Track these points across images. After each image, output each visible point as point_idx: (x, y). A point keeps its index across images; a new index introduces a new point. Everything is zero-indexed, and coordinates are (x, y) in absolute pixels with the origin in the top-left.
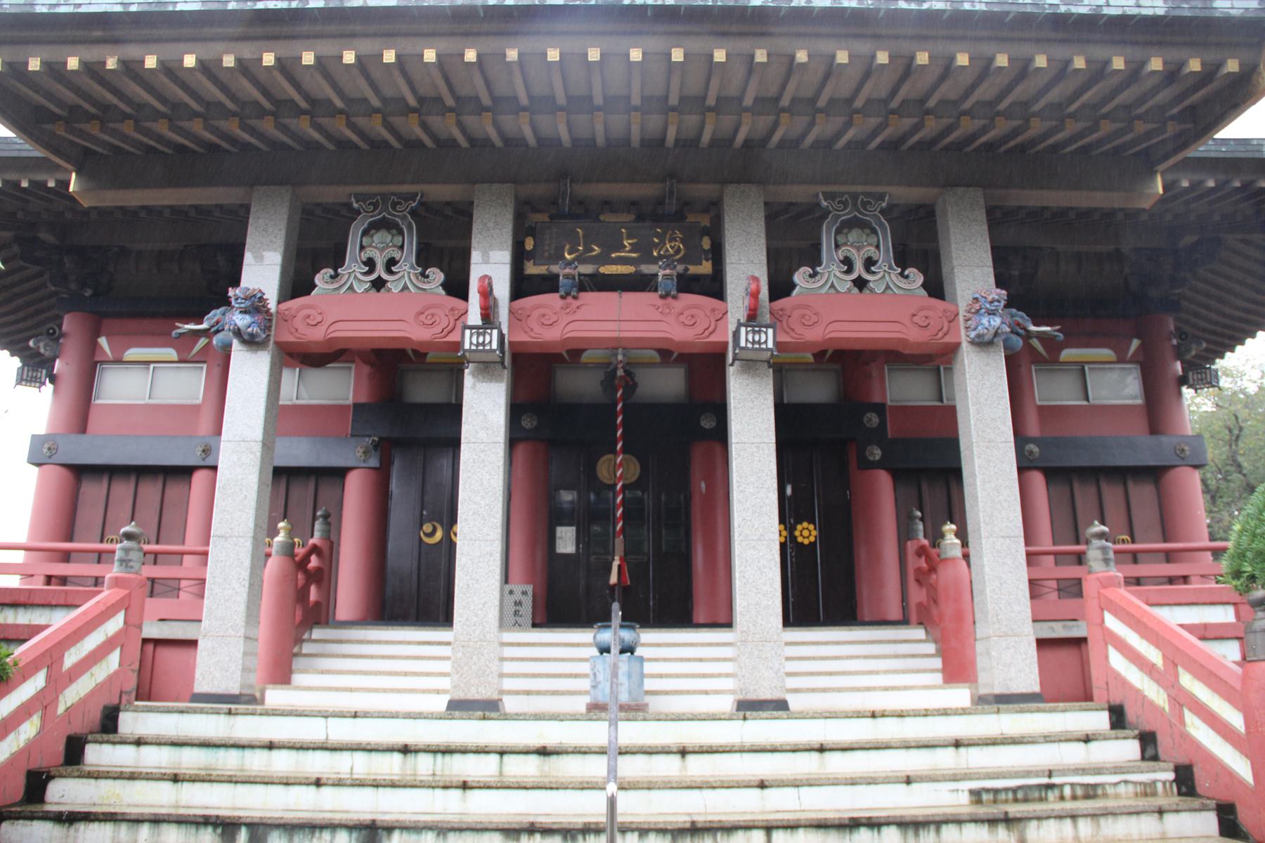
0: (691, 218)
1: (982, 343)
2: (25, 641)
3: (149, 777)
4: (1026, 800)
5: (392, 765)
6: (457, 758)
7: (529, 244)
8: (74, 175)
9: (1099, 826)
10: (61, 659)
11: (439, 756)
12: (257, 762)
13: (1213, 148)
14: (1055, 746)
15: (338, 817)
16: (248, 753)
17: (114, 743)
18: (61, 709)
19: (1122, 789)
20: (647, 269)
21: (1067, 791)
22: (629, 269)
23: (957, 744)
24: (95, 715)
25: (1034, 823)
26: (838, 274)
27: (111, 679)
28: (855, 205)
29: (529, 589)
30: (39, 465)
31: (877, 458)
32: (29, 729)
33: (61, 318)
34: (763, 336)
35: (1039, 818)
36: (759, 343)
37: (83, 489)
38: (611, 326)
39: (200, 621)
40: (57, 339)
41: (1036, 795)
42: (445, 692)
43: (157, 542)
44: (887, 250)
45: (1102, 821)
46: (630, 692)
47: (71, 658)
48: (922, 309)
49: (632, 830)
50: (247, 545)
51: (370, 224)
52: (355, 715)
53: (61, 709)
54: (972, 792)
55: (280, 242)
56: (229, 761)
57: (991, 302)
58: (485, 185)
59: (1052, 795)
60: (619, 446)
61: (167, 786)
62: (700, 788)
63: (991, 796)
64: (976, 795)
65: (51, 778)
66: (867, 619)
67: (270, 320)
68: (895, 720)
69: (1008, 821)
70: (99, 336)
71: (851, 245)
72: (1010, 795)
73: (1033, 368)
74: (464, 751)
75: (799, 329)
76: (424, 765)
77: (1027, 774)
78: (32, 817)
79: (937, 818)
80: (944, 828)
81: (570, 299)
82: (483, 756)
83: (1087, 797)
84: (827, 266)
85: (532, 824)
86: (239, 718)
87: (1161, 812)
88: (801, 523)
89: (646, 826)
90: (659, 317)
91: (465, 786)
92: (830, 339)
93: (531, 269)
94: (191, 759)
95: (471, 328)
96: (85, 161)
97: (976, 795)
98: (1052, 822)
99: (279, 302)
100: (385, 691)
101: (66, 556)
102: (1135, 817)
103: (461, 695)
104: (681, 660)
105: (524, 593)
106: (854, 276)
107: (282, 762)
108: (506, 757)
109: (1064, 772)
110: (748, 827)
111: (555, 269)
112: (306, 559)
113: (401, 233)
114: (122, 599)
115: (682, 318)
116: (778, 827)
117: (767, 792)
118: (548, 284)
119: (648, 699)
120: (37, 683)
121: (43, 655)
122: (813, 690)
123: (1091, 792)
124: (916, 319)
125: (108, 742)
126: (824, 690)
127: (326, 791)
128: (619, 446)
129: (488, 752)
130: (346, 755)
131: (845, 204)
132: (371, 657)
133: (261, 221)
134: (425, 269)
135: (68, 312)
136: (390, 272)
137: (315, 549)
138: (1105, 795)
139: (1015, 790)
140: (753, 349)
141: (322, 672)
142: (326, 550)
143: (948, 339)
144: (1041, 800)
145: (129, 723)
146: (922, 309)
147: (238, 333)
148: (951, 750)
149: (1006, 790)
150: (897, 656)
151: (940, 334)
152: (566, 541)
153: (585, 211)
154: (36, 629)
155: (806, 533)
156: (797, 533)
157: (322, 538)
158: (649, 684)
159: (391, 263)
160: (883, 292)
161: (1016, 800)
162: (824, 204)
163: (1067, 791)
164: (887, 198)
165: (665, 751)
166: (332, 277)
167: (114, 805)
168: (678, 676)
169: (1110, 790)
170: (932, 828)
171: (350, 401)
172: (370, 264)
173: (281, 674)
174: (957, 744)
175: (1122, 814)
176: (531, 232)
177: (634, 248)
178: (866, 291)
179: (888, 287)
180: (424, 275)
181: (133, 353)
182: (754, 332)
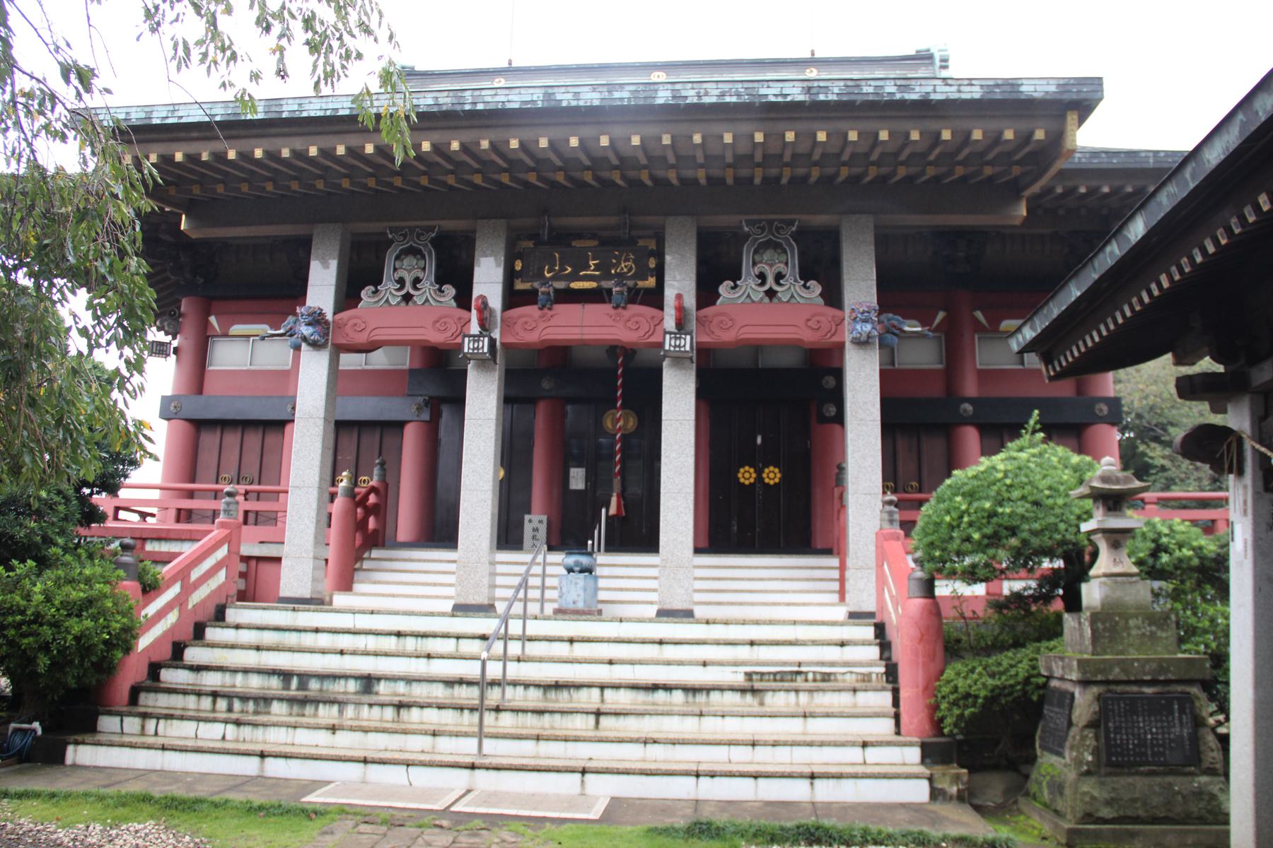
0: (641, 243)
1: (862, 343)
2: (170, 562)
3: (242, 647)
4: (782, 680)
5: (390, 643)
6: (430, 640)
7: (518, 266)
8: (184, 217)
9: (813, 697)
10: (189, 575)
11: (419, 639)
12: (308, 640)
13: (1106, 160)
14: (820, 647)
15: (348, 672)
16: (303, 634)
17: (223, 627)
18: (190, 606)
19: (848, 677)
20: (606, 284)
21: (810, 676)
22: (593, 285)
23: (752, 643)
24: (211, 610)
25: (770, 694)
26: (753, 286)
27: (220, 587)
28: (770, 229)
29: (545, 518)
30: (168, 419)
31: (833, 414)
32: (172, 617)
33: (180, 301)
34: (683, 342)
35: (774, 691)
36: (679, 346)
37: (201, 439)
38: (577, 330)
39: (283, 543)
40: (176, 320)
41: (789, 677)
43: (259, 484)
44: (794, 266)
45: (815, 694)
46: (585, 601)
47: (195, 574)
48: (815, 315)
49: (520, 685)
50: (314, 494)
51: (401, 250)
52: (372, 613)
53: (190, 606)
54: (747, 674)
55: (336, 253)
56: (292, 639)
57: (862, 313)
58: (485, 221)
59: (799, 678)
60: (619, 404)
61: (253, 653)
62: (571, 662)
63: (759, 677)
64: (749, 676)
65: (186, 646)
66: (819, 547)
67: (328, 329)
68: (722, 626)
69: (754, 691)
70: (209, 316)
71: (766, 263)
72: (772, 677)
73: (976, 336)
74: (435, 636)
75: (718, 332)
76: (410, 644)
77: (785, 664)
78: (177, 667)
81: (546, 310)
82: (446, 639)
83: (823, 680)
84: (745, 280)
86: (300, 613)
87: (855, 691)
88: (768, 467)
90: (612, 323)
91: (429, 656)
92: (742, 339)
93: (520, 285)
94: (269, 638)
95: (469, 336)
96: (191, 207)
97: (749, 676)
98: (782, 694)
99: (335, 314)
100: (418, 597)
101: (191, 494)
102: (837, 693)
103: (462, 601)
104: (641, 578)
105: (540, 522)
106: (766, 288)
107: (324, 640)
108: (460, 640)
110: (590, 686)
111: (536, 285)
112: (366, 497)
113: (423, 257)
114: (226, 536)
115: (629, 324)
116: (608, 687)
117: (614, 667)
118: (529, 298)
119: (600, 606)
120: (175, 590)
121: (178, 573)
122: (732, 604)
123: (826, 677)
124: (810, 323)
125: (219, 626)
126: (741, 604)
127: (347, 658)
128: (619, 404)
129: (449, 637)
130: (363, 637)
131: (763, 229)
132: (412, 572)
133: (320, 251)
134: (441, 286)
135: (185, 296)
136: (416, 289)
137: (373, 490)
138: (836, 680)
139: (775, 674)
140: (675, 351)
141: (375, 583)
142: (382, 490)
143: (836, 339)
144: (792, 681)
145: (232, 615)
146: (815, 315)
147: (305, 339)
148: (748, 647)
149: (769, 673)
150: (808, 580)
151: (829, 335)
152: (577, 478)
153: (562, 238)
154: (175, 555)
155: (772, 475)
156: (765, 475)
157: (379, 481)
158: (602, 595)
159: (417, 281)
160: (788, 302)
161: (775, 680)
162: (746, 229)
163: (810, 676)
164: (797, 223)
165: (560, 640)
166: (374, 293)
167: (222, 661)
168: (634, 590)
169: (839, 677)
170: (704, 693)
171: (407, 367)
172: (401, 282)
173: (346, 584)
174: (752, 643)
176: (520, 256)
177: (597, 268)
178: (775, 300)
179: (792, 296)
180: (441, 290)
181: (237, 329)
182: (676, 338)
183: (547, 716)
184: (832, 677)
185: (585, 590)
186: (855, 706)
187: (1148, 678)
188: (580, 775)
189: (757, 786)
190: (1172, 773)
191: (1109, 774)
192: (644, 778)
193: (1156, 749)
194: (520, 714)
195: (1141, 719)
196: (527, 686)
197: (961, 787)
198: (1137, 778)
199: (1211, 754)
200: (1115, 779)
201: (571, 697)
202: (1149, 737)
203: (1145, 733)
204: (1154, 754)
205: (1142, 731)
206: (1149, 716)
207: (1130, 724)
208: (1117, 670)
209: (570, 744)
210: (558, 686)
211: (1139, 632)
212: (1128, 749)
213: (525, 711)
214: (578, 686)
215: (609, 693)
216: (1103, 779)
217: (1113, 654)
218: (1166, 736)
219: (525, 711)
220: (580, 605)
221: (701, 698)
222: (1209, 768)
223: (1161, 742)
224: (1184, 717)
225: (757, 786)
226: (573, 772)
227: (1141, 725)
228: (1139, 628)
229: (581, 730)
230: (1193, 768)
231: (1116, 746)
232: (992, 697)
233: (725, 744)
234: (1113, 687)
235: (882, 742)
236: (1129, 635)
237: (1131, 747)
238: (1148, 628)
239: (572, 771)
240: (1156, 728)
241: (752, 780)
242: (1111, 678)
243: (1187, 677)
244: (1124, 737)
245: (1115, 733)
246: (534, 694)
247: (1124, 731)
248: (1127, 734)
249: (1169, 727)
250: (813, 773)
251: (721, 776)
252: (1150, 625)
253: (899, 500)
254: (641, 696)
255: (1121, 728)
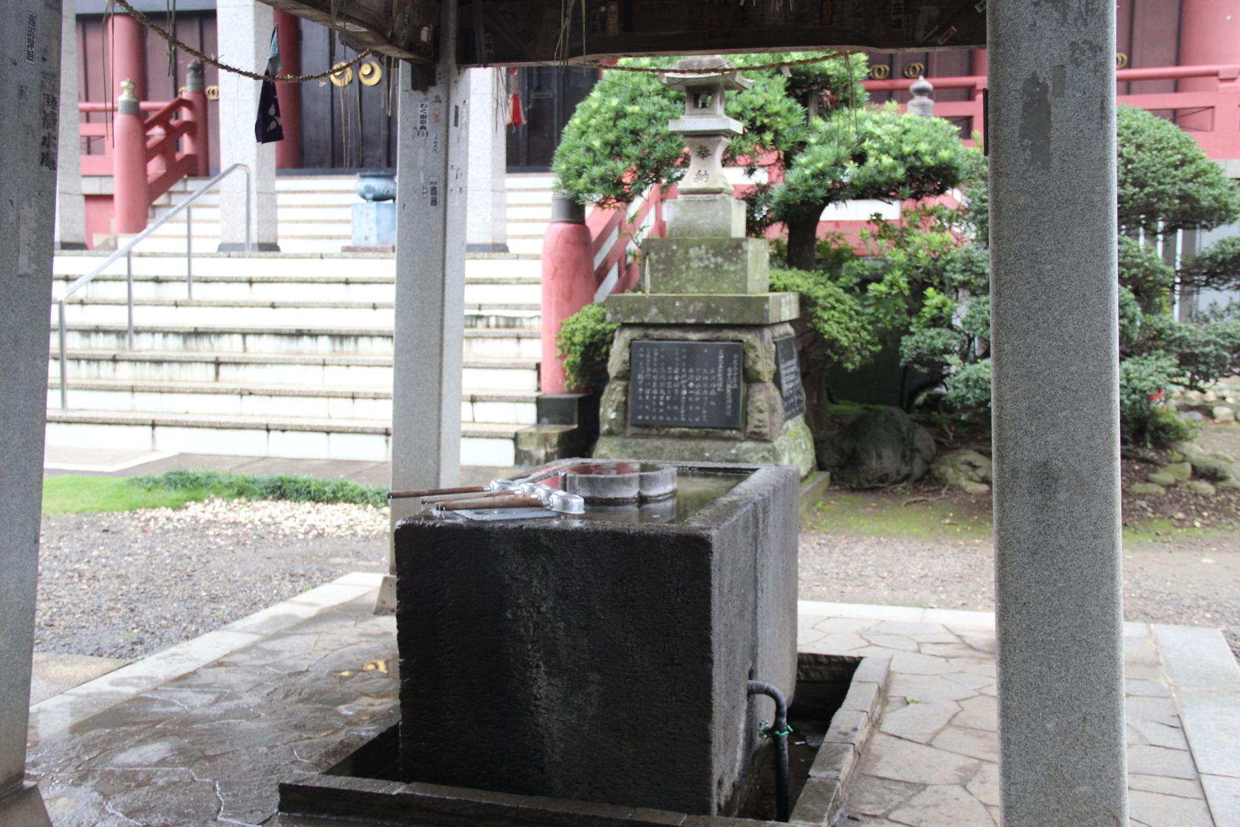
21: (493, 321)
42: (218, 237)
46: (379, 236)
49: (159, 332)
59: (481, 323)
62: (232, 306)
79: (355, 333)
80: (361, 340)
83: (507, 326)
85: (97, 327)
87: (519, 338)
89: (166, 330)
109: (490, 306)
116: (249, 334)
123: (511, 323)
127: (88, 309)
142: (198, 104)
163: (493, 321)
169: (526, 323)
170: (352, 339)
175: (489, 337)
183: (165, 366)
184: (518, 323)
185: (378, 222)
186: (519, 356)
187: (692, 321)
188: (150, 428)
189: (329, 442)
190: (707, 437)
191: (635, 436)
192: (214, 431)
193: (691, 408)
194: (138, 364)
195: (676, 371)
196: (166, 333)
197: (549, 450)
198: (668, 441)
199: (759, 416)
200: (641, 441)
201: (212, 345)
202: (685, 392)
203: (680, 389)
204: (687, 414)
205: (677, 385)
206: (687, 368)
207: (663, 377)
208: (654, 311)
209: (166, 397)
210: (197, 333)
211: (702, 265)
212: (658, 406)
213: (142, 361)
214: (220, 333)
215: (250, 340)
216: (627, 441)
217: (666, 291)
218: (706, 392)
219: (142, 361)
220: (373, 242)
221: (349, 345)
222: (753, 433)
223: (697, 399)
224: (729, 369)
225: (329, 442)
226: (143, 425)
227: (677, 378)
228: (701, 260)
229: (201, 382)
230: (734, 432)
231: (644, 402)
232: (591, 344)
233: (323, 396)
234: (651, 332)
235: (492, 397)
236: (688, 267)
237: (661, 404)
238: (713, 260)
239: (142, 424)
240: (695, 382)
241: (324, 435)
242: (646, 320)
243: (740, 321)
244: (655, 392)
245: (645, 387)
246: (174, 343)
247: (655, 385)
248: (659, 390)
249: (709, 382)
250: (153, 421)
251: (292, 430)
252: (715, 255)
253: (936, 87)
254: (285, 344)
255: (652, 381)
